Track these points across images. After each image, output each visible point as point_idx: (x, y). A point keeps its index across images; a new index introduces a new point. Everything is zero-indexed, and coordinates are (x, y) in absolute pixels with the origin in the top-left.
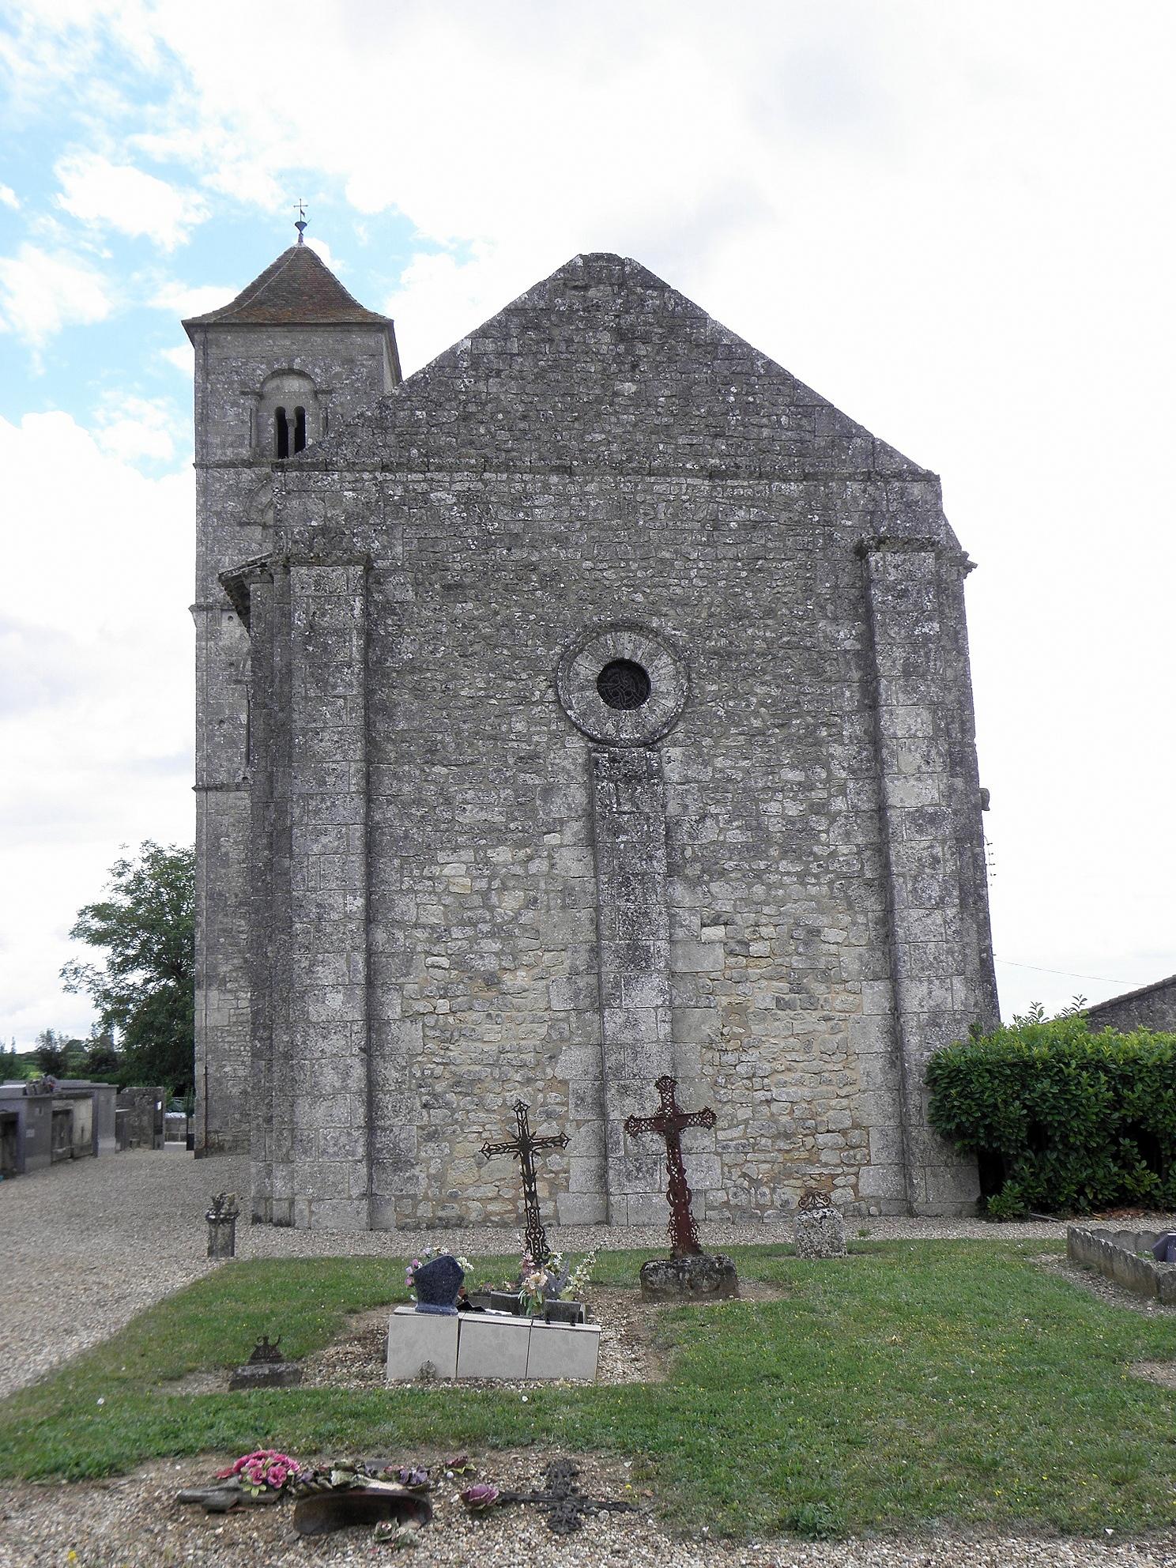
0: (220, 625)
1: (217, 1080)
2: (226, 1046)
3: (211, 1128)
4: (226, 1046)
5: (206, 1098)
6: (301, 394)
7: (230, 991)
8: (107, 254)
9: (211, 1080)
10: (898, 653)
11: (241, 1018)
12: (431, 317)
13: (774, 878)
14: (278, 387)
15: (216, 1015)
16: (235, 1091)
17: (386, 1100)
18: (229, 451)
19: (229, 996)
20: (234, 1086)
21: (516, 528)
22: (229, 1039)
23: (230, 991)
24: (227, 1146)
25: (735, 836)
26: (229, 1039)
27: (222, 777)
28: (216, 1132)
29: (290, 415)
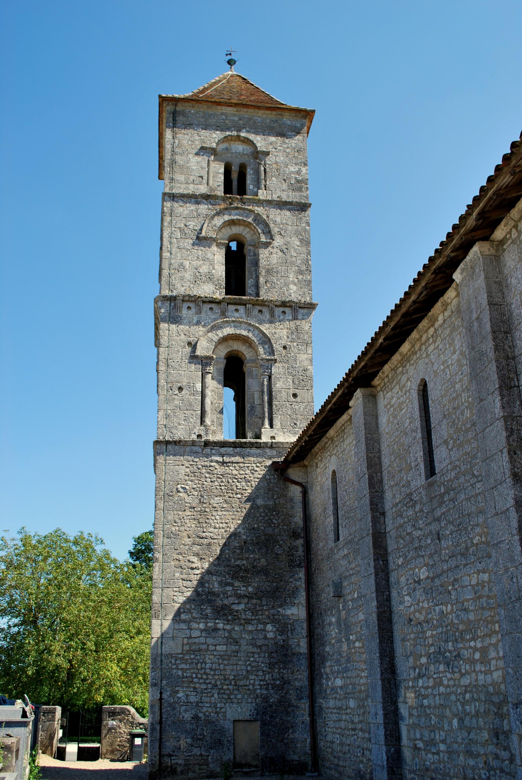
0: (181, 311)
1: (170, 705)
2: (180, 673)
3: (165, 751)
4: (180, 673)
5: (161, 722)
6: (244, 154)
7: (184, 621)
8: (41, 775)
9: (165, 705)
11: (193, 647)
12: (370, 341)
14: (227, 149)
15: (171, 643)
16: (188, 716)
17: (391, 545)
18: (191, 186)
19: (183, 626)
20: (186, 711)
22: (183, 666)
23: (184, 621)
24: (179, 769)
26: (183, 666)
27: (180, 434)
28: (170, 756)
29: (235, 169)
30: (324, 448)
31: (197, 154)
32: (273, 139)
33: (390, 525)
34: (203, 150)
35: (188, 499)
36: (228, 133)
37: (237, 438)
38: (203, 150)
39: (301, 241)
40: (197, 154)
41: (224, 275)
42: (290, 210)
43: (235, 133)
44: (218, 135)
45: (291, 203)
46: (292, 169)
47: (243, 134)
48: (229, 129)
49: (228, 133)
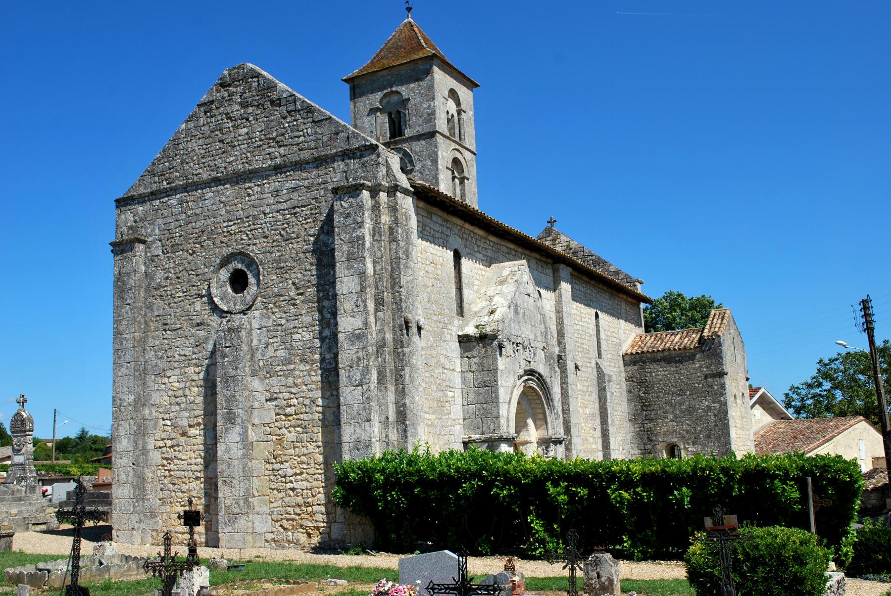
10: (345, 248)
13: (297, 373)
14: (388, 102)
21: (198, 211)
25: (281, 353)
30: (594, 286)
31: (368, 115)
32: (412, 85)
33: (306, 155)
34: (373, 111)
35: (437, 371)
36: (385, 91)
37: (622, 581)
38: (373, 111)
39: (432, 161)
40: (368, 115)
41: (472, 103)
42: (424, 139)
43: (389, 90)
44: (379, 95)
45: (424, 134)
46: (425, 106)
47: (394, 89)
48: (385, 88)
49: (385, 91)
